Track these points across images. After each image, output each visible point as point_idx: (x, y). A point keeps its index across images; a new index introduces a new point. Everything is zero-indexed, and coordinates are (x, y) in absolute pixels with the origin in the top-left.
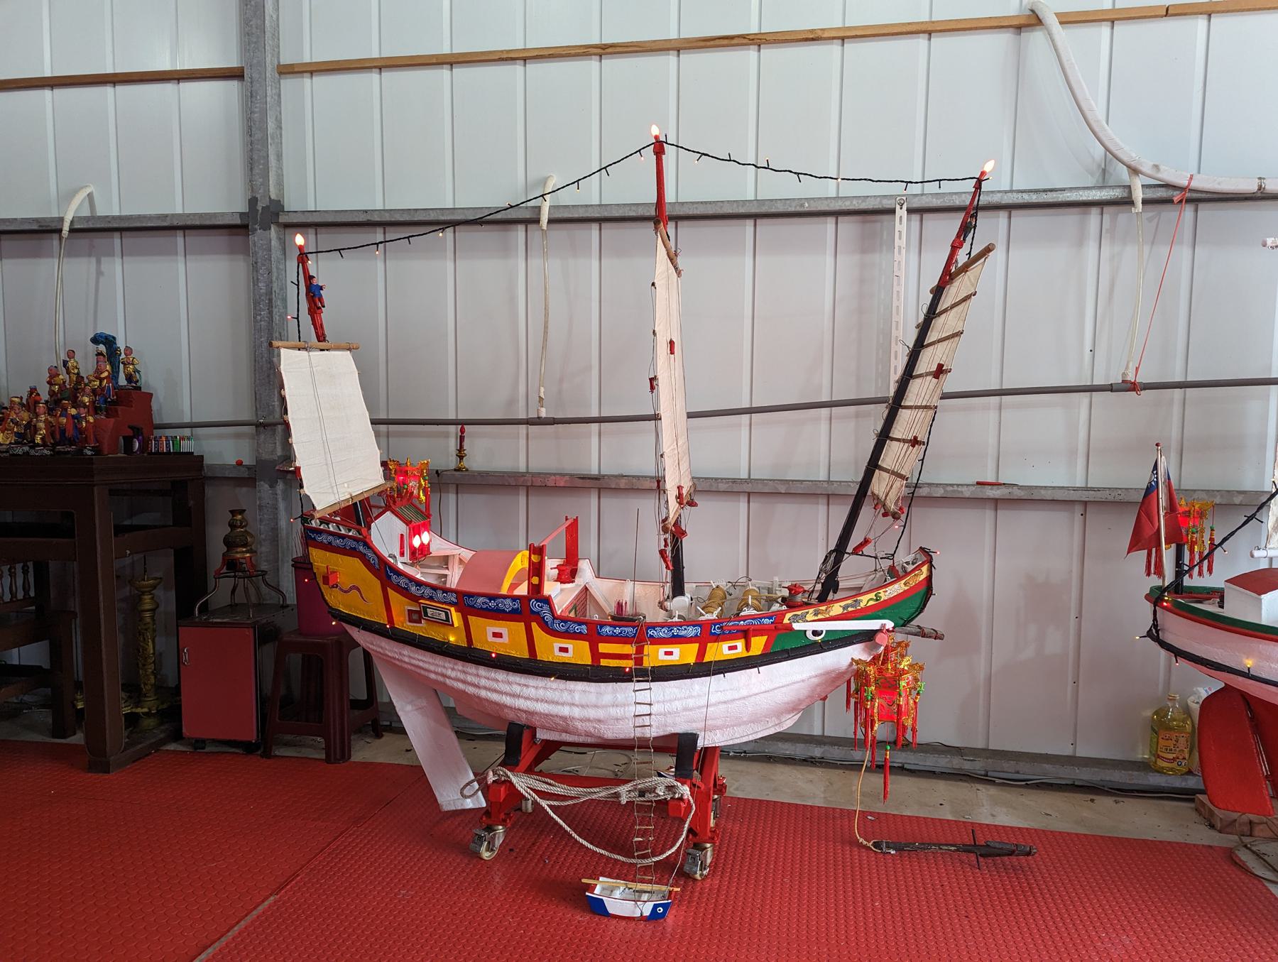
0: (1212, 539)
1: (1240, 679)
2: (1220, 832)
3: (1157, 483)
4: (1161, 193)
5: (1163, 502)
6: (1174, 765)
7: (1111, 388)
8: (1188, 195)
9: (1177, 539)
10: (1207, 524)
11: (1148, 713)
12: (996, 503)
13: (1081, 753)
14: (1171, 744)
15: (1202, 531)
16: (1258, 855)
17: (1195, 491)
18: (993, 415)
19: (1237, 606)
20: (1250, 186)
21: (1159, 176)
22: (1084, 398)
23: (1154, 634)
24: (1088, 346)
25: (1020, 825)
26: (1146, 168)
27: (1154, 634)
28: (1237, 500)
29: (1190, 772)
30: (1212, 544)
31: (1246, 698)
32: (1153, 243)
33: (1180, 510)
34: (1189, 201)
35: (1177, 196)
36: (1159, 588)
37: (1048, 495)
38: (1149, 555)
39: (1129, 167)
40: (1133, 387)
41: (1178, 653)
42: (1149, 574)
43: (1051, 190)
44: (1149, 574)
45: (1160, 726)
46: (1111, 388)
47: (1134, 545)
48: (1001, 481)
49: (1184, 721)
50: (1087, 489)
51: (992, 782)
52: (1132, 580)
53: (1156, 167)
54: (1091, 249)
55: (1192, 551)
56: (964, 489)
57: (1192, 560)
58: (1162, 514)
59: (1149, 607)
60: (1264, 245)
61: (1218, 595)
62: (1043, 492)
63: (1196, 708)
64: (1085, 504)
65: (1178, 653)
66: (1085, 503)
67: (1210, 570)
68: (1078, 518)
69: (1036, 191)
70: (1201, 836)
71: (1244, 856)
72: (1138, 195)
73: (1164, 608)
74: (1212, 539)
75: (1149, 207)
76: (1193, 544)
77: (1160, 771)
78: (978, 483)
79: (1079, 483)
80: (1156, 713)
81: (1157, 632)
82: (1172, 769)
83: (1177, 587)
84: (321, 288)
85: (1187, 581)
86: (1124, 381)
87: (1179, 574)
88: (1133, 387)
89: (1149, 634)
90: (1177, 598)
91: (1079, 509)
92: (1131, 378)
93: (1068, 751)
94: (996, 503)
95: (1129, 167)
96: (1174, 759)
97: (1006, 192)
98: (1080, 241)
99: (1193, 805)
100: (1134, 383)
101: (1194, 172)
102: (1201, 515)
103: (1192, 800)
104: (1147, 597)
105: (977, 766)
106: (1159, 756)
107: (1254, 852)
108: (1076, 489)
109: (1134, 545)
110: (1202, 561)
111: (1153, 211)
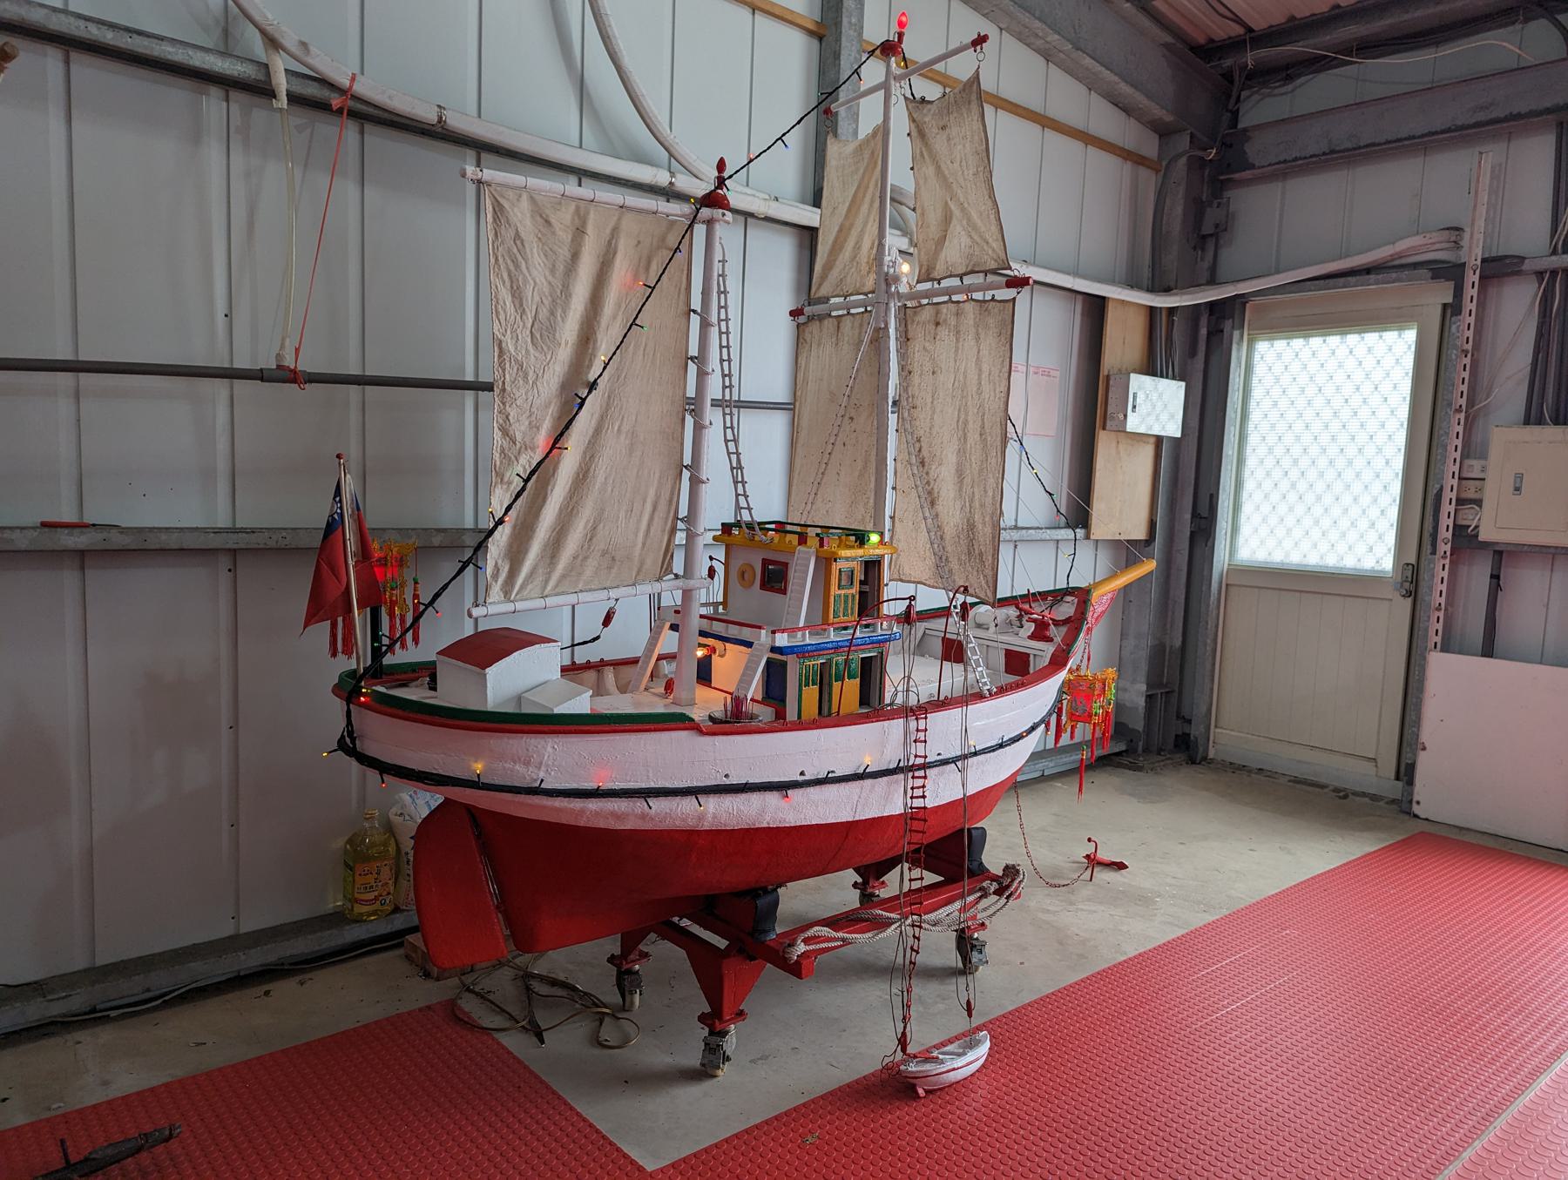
0: (416, 596)
1: (468, 791)
2: (438, 979)
3: (342, 515)
4: (312, 90)
5: (351, 546)
6: (377, 906)
7: (260, 376)
8: (350, 103)
9: (374, 601)
10: (408, 574)
11: (340, 843)
12: (82, 557)
13: (247, 926)
14: (371, 879)
15: (403, 585)
16: (482, 996)
17: (384, 530)
18: (65, 407)
19: (453, 690)
20: (429, 115)
21: (310, 60)
22: (220, 387)
23: (348, 745)
24: (221, 307)
25: (155, 1083)
26: (290, 42)
27: (348, 745)
28: (436, 541)
29: (397, 910)
30: (416, 607)
31: (471, 811)
32: (306, 166)
33: (377, 554)
34: (353, 114)
35: (336, 101)
36: (352, 674)
37: (173, 542)
38: (334, 626)
39: (263, 32)
40: (292, 377)
41: (384, 768)
42: (334, 654)
43: (140, 33)
44: (334, 654)
45: (356, 856)
46: (260, 376)
47: (315, 612)
48: (88, 520)
49: (385, 844)
50: (234, 530)
51: (106, 1019)
52: (308, 667)
53: (304, 44)
54: (213, 153)
55: (392, 615)
56: (16, 535)
57: (392, 627)
58: (351, 563)
59: (339, 705)
60: (464, 175)
61: (428, 672)
62: (164, 537)
63: (408, 845)
64: (232, 553)
65: (384, 768)
66: (234, 552)
67: (416, 640)
68: (224, 578)
69: (113, 26)
70: (420, 994)
71: (469, 1005)
72: (281, 83)
73: (361, 705)
74: (416, 596)
75: (297, 109)
76: (393, 603)
77: (358, 920)
78: (44, 525)
79: (223, 521)
80: (350, 841)
81: (353, 740)
82: (374, 913)
83: (377, 671)
84: (1424, 749)
85: (388, 660)
86: (279, 367)
87: (377, 654)
88: (292, 377)
89: (342, 745)
90: (375, 687)
91: (224, 562)
92: (289, 362)
93: (227, 930)
94: (82, 557)
95: (263, 32)
96: (376, 898)
97: (54, 10)
98: (196, 136)
99: (401, 951)
100: (294, 372)
101: (357, 71)
102: (401, 562)
103: (400, 945)
104: (337, 690)
105: (78, 1001)
106: (357, 901)
107: (477, 994)
108: (218, 531)
109: (312, 617)
110: (405, 632)
111: (300, 117)
